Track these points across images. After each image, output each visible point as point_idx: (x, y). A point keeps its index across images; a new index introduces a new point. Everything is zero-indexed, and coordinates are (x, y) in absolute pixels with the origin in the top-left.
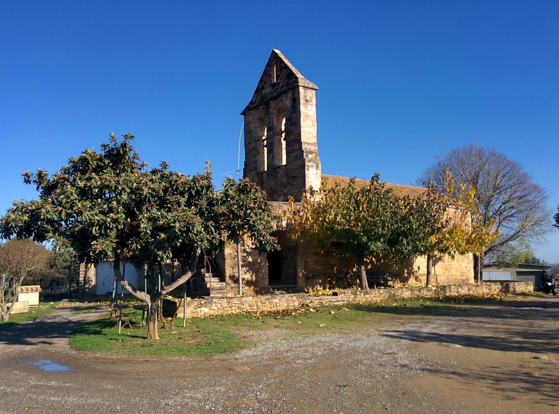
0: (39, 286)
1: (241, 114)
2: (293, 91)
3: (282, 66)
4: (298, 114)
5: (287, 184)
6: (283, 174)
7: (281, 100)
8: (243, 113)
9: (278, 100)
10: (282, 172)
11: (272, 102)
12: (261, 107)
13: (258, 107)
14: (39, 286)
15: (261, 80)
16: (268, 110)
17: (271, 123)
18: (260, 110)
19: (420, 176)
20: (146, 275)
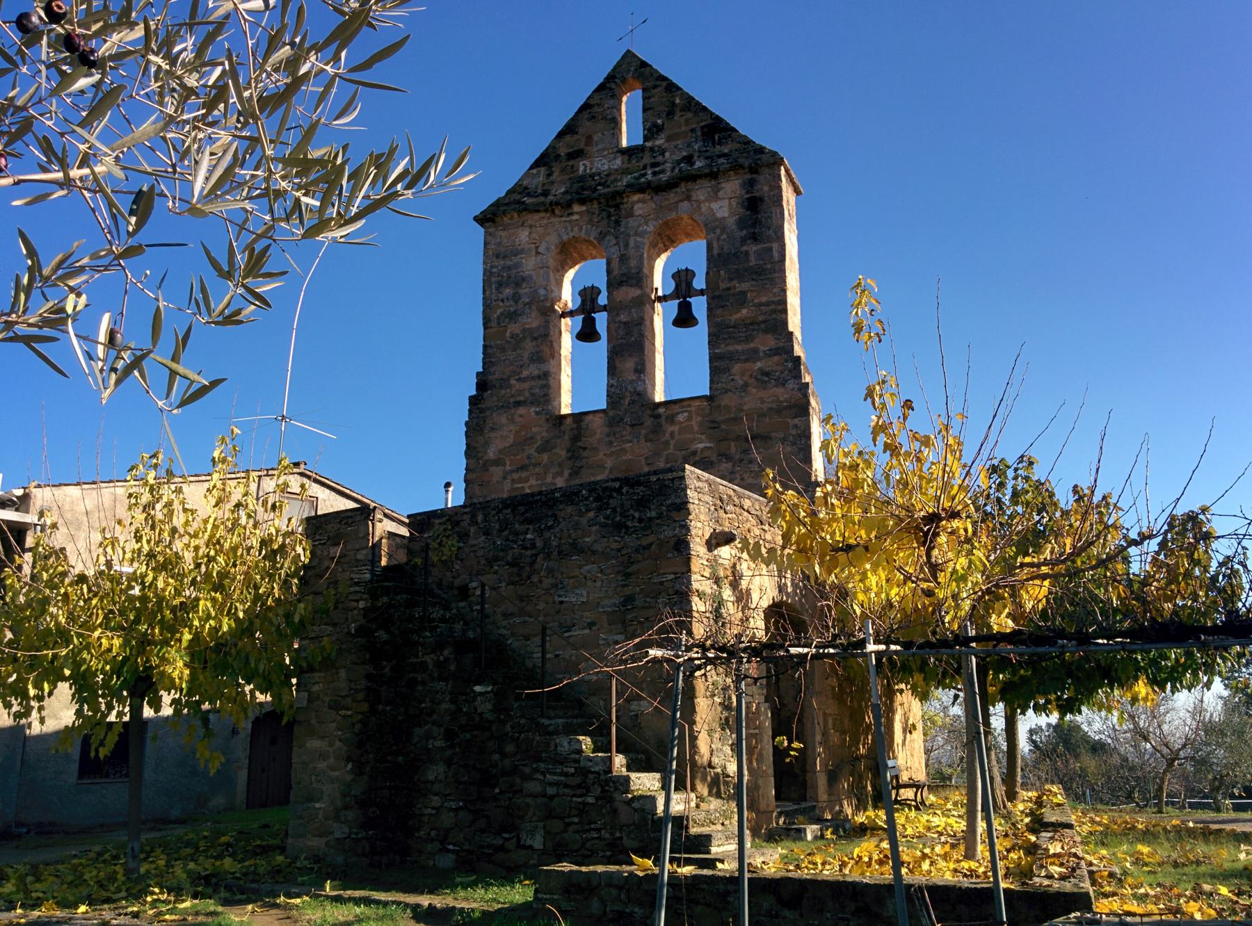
0: (884, 811)
1: (476, 219)
2: (749, 176)
3: (673, 104)
4: (775, 246)
5: (714, 458)
6: (694, 424)
7: (688, 198)
8: (482, 219)
9: (672, 196)
10: (690, 418)
11: (636, 197)
12: (577, 208)
13: (569, 205)
14: (884, 811)
15: (569, 129)
16: (618, 223)
17: (633, 263)
18: (575, 217)
19: (1222, 549)
20: (25, 252)
